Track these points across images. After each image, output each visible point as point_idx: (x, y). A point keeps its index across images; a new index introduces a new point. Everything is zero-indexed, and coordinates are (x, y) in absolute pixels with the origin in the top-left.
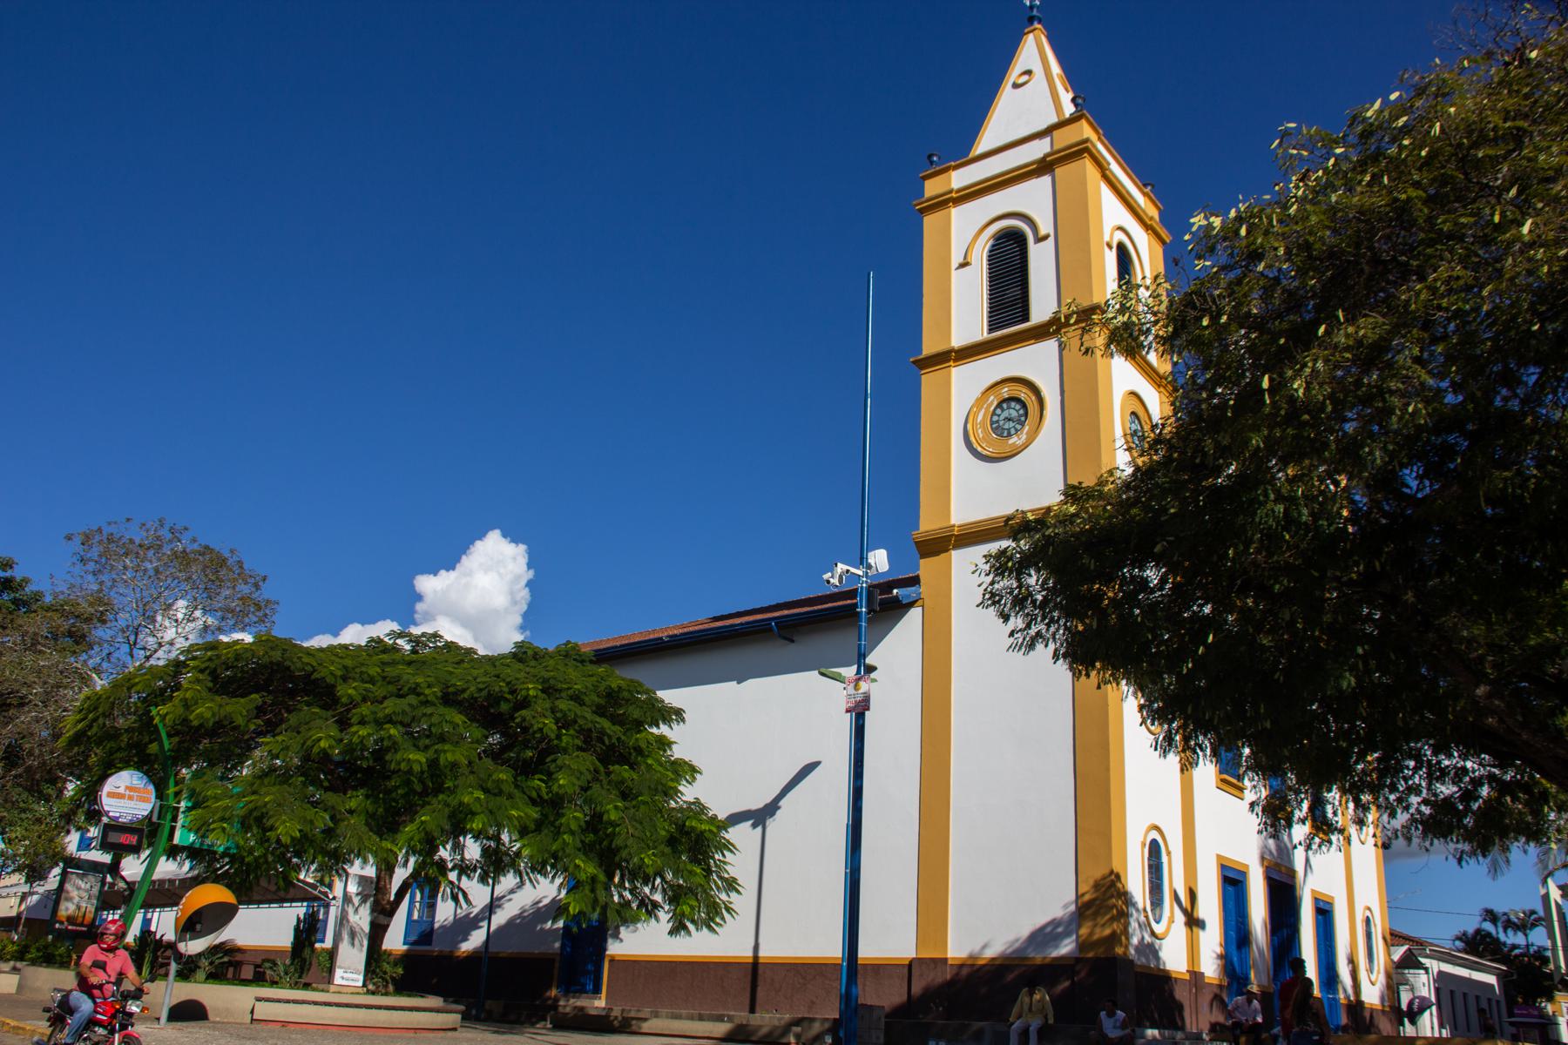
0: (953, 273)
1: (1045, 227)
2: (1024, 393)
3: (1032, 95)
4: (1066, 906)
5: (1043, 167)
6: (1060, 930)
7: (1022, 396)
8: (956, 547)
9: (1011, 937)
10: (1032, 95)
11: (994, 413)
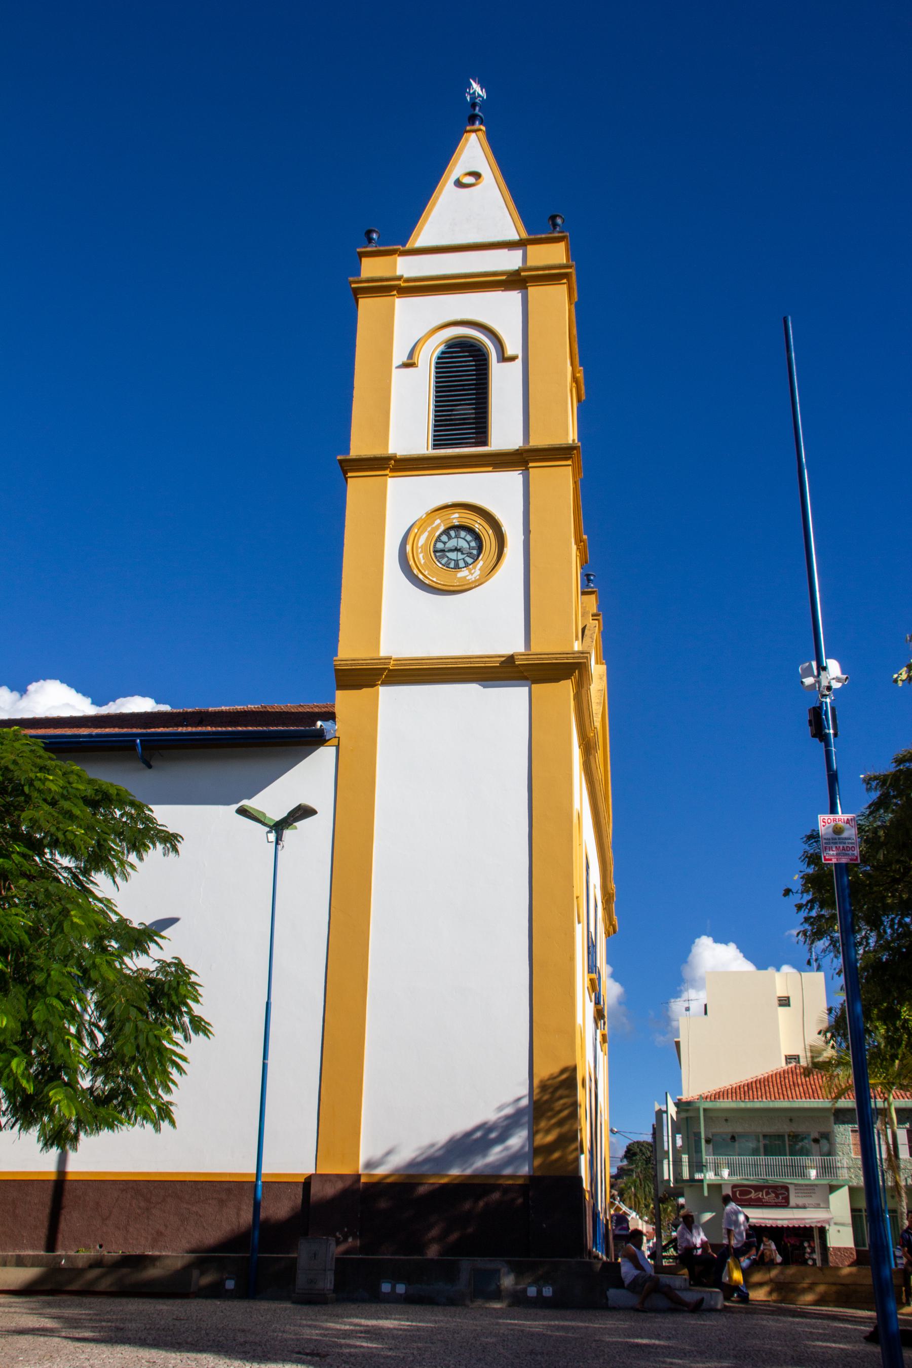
0: (395, 372)
1: (513, 346)
2: (479, 524)
3: (471, 204)
4: (500, 1108)
5: (515, 281)
6: (493, 1135)
7: (477, 527)
8: (384, 683)
9: (425, 1141)
10: (471, 204)
11: (438, 539)
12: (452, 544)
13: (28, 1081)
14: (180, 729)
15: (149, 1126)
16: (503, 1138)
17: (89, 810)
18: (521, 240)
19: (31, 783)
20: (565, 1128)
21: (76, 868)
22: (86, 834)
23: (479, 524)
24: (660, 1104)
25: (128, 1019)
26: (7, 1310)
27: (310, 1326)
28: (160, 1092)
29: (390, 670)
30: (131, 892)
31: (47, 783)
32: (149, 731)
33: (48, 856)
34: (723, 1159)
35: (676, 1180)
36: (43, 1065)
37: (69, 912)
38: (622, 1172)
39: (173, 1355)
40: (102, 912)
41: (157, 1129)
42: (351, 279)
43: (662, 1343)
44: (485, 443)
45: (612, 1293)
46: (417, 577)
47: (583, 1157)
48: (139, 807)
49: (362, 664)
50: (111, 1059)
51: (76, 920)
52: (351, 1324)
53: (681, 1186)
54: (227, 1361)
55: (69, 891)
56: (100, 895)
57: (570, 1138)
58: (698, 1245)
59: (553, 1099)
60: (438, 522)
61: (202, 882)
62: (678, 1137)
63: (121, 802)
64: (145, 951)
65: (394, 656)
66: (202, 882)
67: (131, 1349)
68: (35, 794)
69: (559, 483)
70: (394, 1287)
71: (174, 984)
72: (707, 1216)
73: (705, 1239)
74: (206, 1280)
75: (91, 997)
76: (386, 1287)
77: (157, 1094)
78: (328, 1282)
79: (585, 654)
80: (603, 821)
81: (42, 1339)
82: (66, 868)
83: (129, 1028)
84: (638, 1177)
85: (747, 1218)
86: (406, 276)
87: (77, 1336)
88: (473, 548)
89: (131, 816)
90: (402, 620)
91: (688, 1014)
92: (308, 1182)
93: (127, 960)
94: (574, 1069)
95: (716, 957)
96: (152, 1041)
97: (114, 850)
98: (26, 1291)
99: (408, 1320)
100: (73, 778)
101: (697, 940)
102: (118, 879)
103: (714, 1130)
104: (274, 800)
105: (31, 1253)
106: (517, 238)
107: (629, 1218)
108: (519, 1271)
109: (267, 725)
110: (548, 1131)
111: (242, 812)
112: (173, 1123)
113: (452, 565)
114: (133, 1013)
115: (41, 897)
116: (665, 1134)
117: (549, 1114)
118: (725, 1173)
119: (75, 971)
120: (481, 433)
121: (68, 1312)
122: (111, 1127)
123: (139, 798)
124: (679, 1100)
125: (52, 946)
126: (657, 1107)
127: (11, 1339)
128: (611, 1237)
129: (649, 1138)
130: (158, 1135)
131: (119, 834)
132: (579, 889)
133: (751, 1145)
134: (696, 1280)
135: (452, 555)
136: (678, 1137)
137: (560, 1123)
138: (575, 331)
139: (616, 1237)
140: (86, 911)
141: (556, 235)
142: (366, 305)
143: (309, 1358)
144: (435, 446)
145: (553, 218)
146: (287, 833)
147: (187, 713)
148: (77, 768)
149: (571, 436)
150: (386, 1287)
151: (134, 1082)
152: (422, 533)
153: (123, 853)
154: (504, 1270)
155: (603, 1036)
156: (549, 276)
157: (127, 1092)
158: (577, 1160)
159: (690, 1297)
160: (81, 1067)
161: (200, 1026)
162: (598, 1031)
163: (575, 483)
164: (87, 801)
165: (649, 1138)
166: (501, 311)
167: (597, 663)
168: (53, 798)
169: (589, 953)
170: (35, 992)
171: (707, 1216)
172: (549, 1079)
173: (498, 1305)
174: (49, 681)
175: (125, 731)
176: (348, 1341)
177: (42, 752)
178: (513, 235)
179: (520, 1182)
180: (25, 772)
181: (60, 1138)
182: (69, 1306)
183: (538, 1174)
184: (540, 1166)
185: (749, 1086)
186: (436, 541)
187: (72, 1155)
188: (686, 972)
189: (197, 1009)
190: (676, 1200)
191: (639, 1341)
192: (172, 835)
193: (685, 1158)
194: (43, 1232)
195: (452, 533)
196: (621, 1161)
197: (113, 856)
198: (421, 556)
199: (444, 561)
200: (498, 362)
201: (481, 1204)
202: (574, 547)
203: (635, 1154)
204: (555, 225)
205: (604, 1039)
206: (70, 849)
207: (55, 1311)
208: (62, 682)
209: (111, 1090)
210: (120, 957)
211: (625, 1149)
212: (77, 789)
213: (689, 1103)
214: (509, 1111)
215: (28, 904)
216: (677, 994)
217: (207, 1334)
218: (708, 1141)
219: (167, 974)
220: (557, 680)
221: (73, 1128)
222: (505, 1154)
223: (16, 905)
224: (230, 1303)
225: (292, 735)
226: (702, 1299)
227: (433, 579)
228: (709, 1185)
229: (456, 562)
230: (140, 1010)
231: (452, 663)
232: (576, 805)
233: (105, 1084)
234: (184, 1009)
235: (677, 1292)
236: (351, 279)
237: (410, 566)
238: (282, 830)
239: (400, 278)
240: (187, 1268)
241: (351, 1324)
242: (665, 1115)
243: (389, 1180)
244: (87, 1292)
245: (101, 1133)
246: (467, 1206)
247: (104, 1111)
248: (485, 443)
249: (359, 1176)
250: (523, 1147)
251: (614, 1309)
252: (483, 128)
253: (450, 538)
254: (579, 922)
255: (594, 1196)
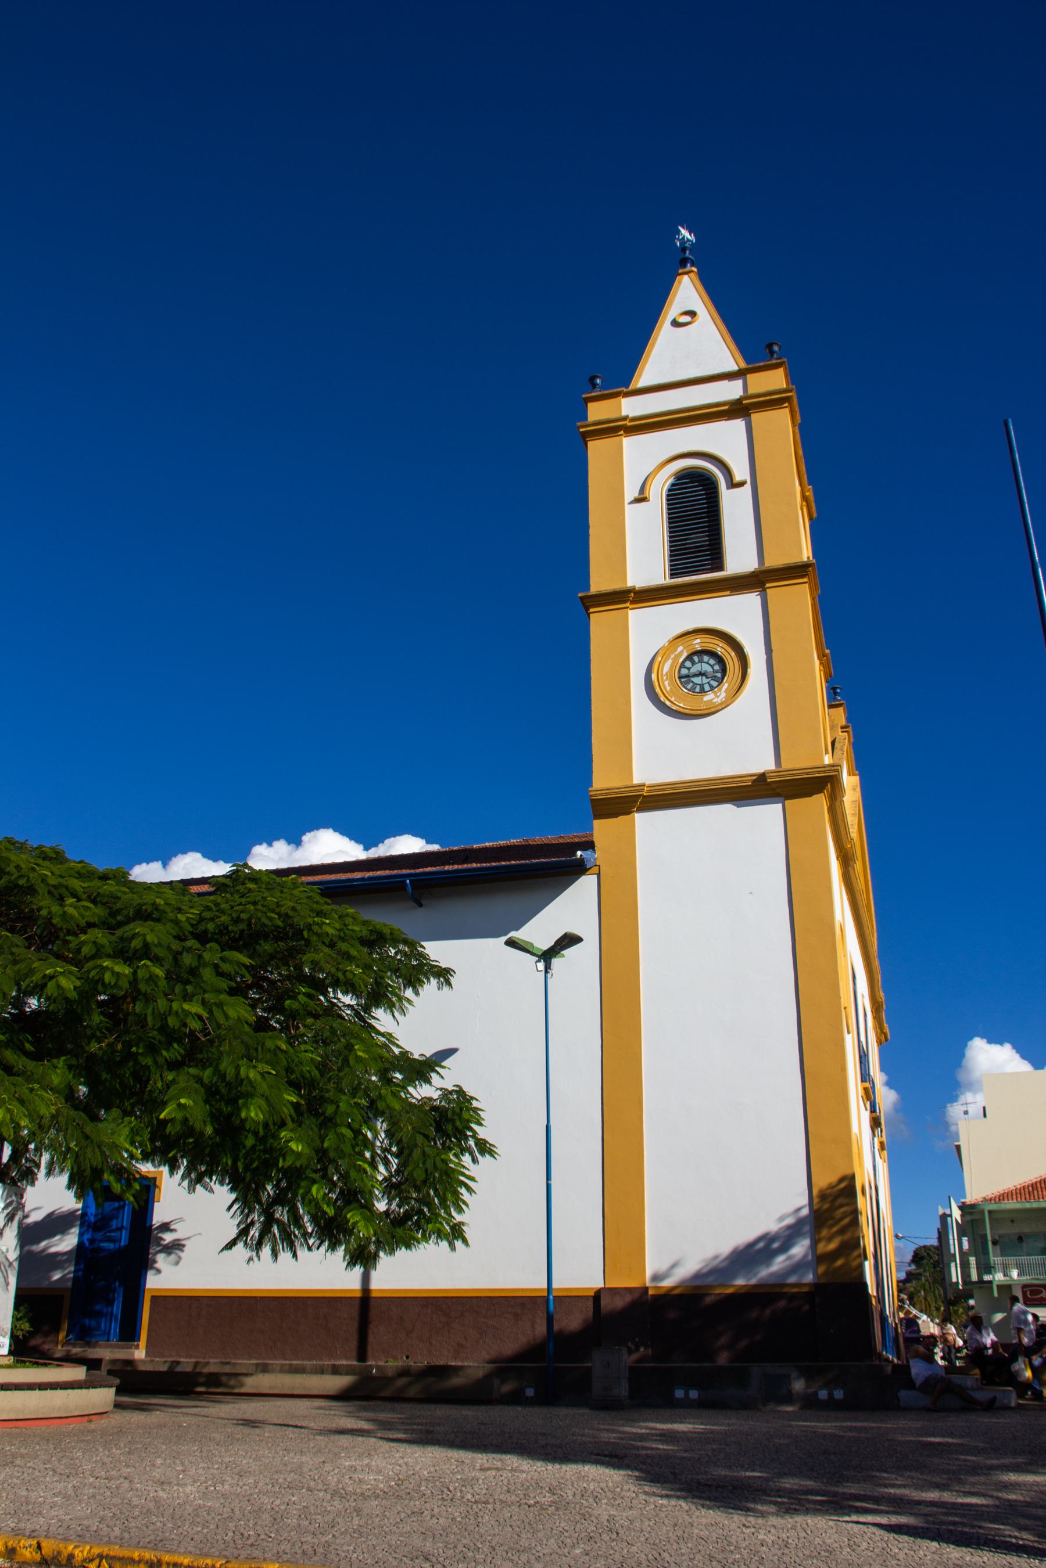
0: (628, 508)
1: (741, 473)
2: (720, 648)
3: (689, 343)
4: (781, 1219)
5: (737, 410)
6: (776, 1245)
7: (719, 650)
8: (641, 810)
9: (709, 1253)
10: (689, 343)
11: (682, 666)
12: (696, 669)
13: (328, 1205)
14: (447, 868)
15: (444, 1244)
16: (785, 1248)
17: (366, 950)
18: (740, 370)
19: (309, 927)
20: (847, 1236)
21: (358, 1005)
22: (364, 973)
23: (720, 648)
24: (943, 1208)
25: (416, 1145)
26: (327, 1412)
27: (608, 1430)
28: (454, 1213)
29: (644, 797)
30: (412, 1025)
31: (324, 927)
32: (417, 871)
33: (332, 995)
34: (1011, 1260)
35: (964, 1283)
36: (342, 1192)
37: (353, 1046)
38: (910, 1276)
39: (480, 1456)
40: (385, 1046)
41: (453, 1248)
42: (579, 424)
43: (955, 1441)
44: (721, 568)
45: (903, 1394)
46: (664, 704)
47: (867, 1263)
48: (412, 944)
49: (617, 793)
50: (404, 1183)
51: (360, 1053)
52: (647, 1428)
53: (970, 1288)
54: (530, 1461)
55: (352, 1027)
56: (382, 1029)
57: (852, 1246)
58: (988, 1345)
59: (834, 1207)
60: (680, 648)
61: (479, 1013)
62: (965, 1240)
63: (395, 941)
64: (428, 1081)
65: (647, 783)
66: (479, 1013)
67: (441, 1449)
68: (314, 938)
69: (798, 601)
70: (687, 1394)
71: (457, 1110)
72: (999, 1317)
73: (995, 1338)
74: (507, 1388)
75: (381, 1126)
76: (679, 1393)
77: (450, 1215)
78: (623, 1390)
79: (836, 767)
80: (867, 931)
81: (360, 1439)
82: (349, 1006)
83: (417, 1153)
84: (927, 1280)
85: (1035, 1317)
86: (631, 415)
87: (391, 1437)
88: (717, 672)
89: (405, 954)
90: (653, 748)
91: (965, 1116)
92: (598, 1295)
93: (411, 1089)
94: (852, 1178)
95: (991, 1059)
96: (440, 1165)
97: (391, 986)
98: (342, 1396)
99: (702, 1424)
100: (348, 920)
101: (970, 1043)
102: (396, 1014)
103: (1000, 1232)
104: (541, 930)
105: (345, 1362)
106: (735, 368)
107: (920, 1322)
108: (809, 1375)
109: (529, 858)
110: (830, 1239)
111: (511, 943)
112: (465, 1241)
113: (698, 689)
114: (420, 1139)
115: (327, 1034)
116: (951, 1237)
117: (830, 1222)
118: (1015, 1274)
119: (364, 1102)
120: (716, 560)
121: (382, 1416)
122: (408, 1246)
123: (411, 936)
124: (963, 1203)
125: (340, 1080)
126: (941, 1211)
127: (332, 1437)
128: (901, 1340)
129: (934, 1242)
130: (453, 1254)
131: (396, 971)
132: (846, 998)
133: (1040, 1245)
134: (988, 1379)
135: (697, 680)
136: (965, 1240)
137: (842, 1231)
138: (800, 452)
139: (906, 1340)
140: (370, 1045)
141: (774, 362)
142: (596, 448)
143: (607, 1459)
144: (672, 576)
145: (770, 346)
146: (556, 962)
147: (452, 851)
148: (351, 911)
149: (806, 553)
150: (679, 1393)
151: (428, 1203)
152: (666, 660)
153: (400, 989)
154: (794, 1375)
155: (882, 1144)
156: (770, 402)
157: (420, 1212)
158: (861, 1267)
159: (982, 1395)
160: (377, 1192)
161: (485, 1148)
162: (876, 1139)
163: (813, 599)
164: (363, 942)
165: (934, 1242)
166: (726, 440)
167: (849, 774)
168: (331, 940)
169: (861, 1062)
170: (327, 1123)
171: (999, 1317)
172: (827, 1189)
173: (790, 1409)
174: (322, 830)
175: (395, 872)
176: (644, 1444)
177: (318, 898)
178: (732, 366)
179: (805, 1289)
180: (304, 917)
181: (362, 1258)
182: (382, 1411)
183: (823, 1281)
184: (825, 1273)
185: (1034, 1186)
186: (680, 667)
187: (375, 1275)
188: (961, 1076)
189: (482, 1132)
190: (966, 1302)
191: (932, 1439)
192: (445, 969)
193: (972, 1260)
194: (354, 1344)
195: (696, 658)
196: (909, 1265)
197: (392, 993)
198: (666, 683)
199: (689, 686)
200: (728, 488)
201: (768, 1312)
202: (817, 662)
203: (922, 1258)
204: (772, 353)
205: (882, 1146)
206: (350, 987)
207: (370, 1415)
208: (335, 831)
209: (406, 1211)
210: (404, 1088)
211: (912, 1254)
212: (353, 931)
213: (973, 1206)
214: (790, 1221)
215: (317, 1042)
216: (954, 1099)
217: (511, 1437)
218: (995, 1243)
219: (449, 1101)
220: (810, 795)
221: (373, 1247)
222: (787, 1263)
223: (305, 1043)
224: (531, 1409)
225: (554, 866)
226: (994, 1399)
227: (680, 705)
228: (998, 1286)
229: (702, 686)
230: (426, 1137)
231: (704, 785)
232: (838, 917)
233: (399, 1206)
234: (469, 1133)
235: (972, 1393)
236: (579, 424)
237: (656, 694)
238: (550, 959)
239: (625, 418)
240: (488, 1377)
241: (647, 1428)
242: (949, 1219)
243: (676, 1292)
244: (398, 1398)
245: (398, 1253)
246: (754, 1314)
247: (401, 1232)
248: (721, 568)
249: (646, 1289)
250: (805, 1256)
251: (906, 1409)
252: (694, 269)
253: (693, 663)
254: (849, 1032)
255: (881, 1300)
